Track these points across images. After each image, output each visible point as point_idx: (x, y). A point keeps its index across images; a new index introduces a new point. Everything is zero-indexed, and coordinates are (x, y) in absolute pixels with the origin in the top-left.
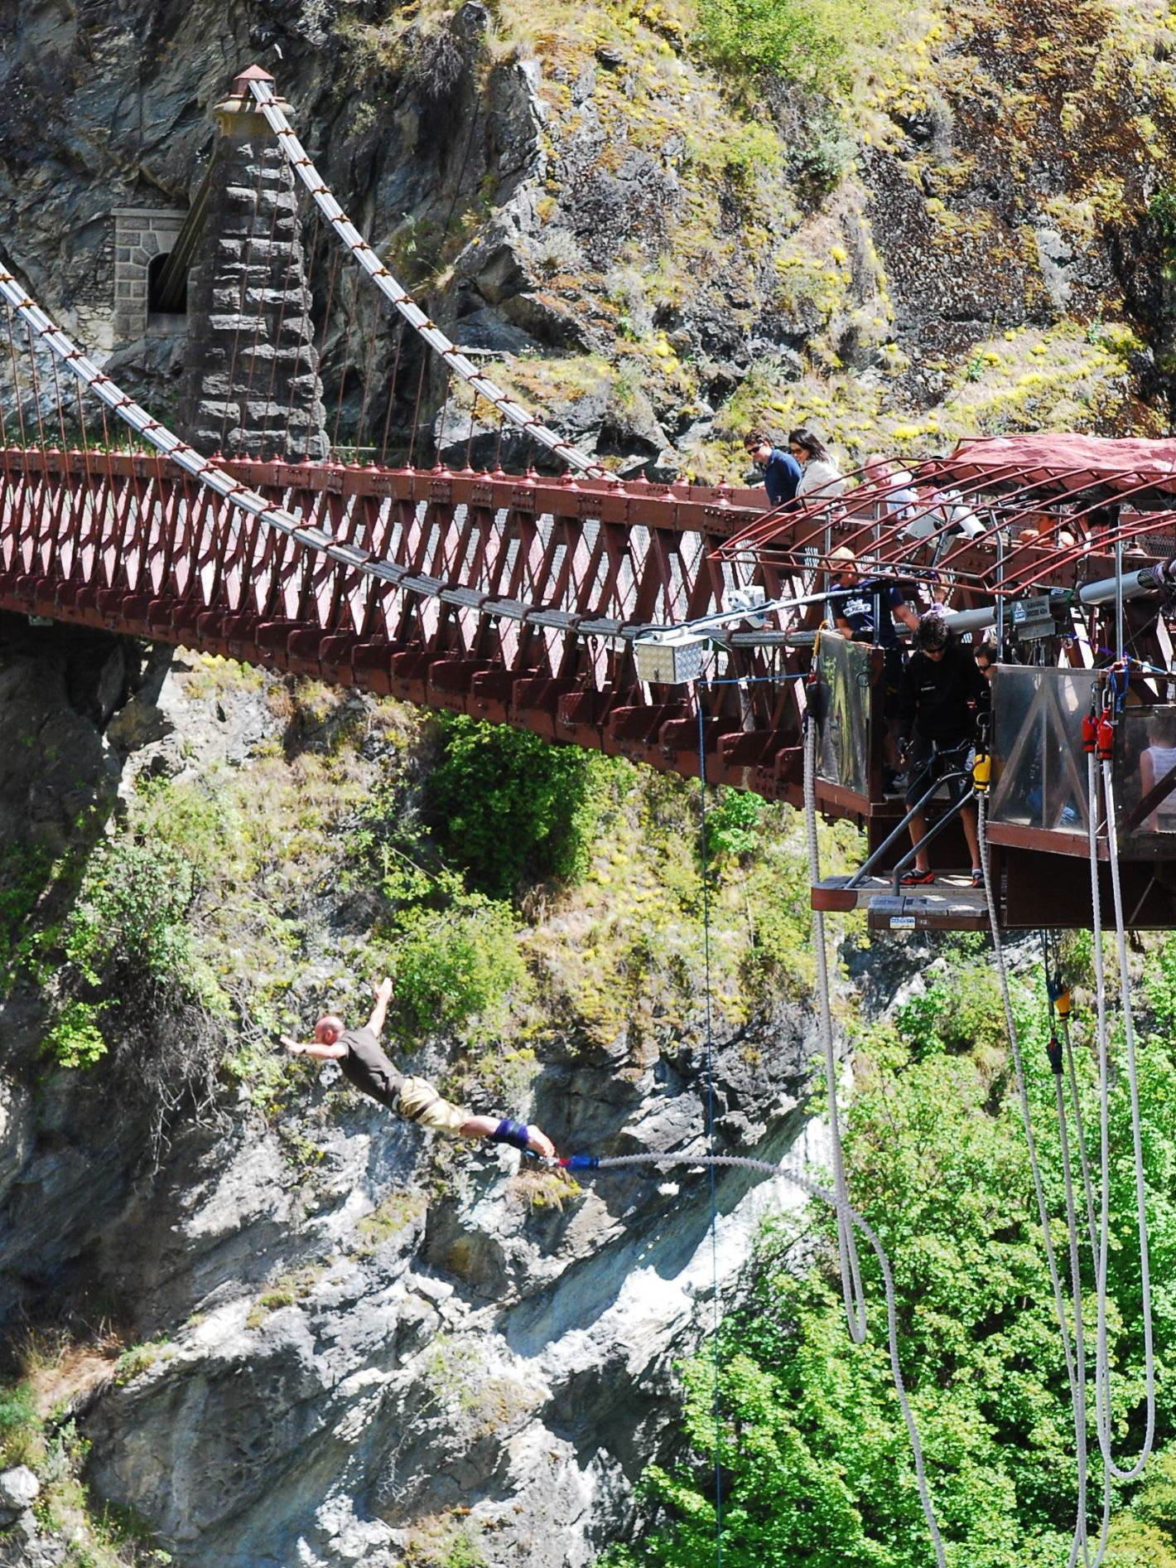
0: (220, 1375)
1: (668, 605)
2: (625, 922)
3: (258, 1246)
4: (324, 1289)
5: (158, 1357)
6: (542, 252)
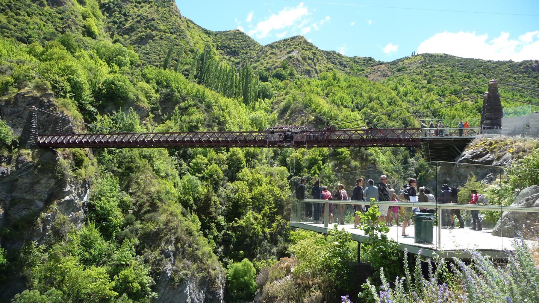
0: (68, 201)
1: (28, 92)
5: (63, 200)
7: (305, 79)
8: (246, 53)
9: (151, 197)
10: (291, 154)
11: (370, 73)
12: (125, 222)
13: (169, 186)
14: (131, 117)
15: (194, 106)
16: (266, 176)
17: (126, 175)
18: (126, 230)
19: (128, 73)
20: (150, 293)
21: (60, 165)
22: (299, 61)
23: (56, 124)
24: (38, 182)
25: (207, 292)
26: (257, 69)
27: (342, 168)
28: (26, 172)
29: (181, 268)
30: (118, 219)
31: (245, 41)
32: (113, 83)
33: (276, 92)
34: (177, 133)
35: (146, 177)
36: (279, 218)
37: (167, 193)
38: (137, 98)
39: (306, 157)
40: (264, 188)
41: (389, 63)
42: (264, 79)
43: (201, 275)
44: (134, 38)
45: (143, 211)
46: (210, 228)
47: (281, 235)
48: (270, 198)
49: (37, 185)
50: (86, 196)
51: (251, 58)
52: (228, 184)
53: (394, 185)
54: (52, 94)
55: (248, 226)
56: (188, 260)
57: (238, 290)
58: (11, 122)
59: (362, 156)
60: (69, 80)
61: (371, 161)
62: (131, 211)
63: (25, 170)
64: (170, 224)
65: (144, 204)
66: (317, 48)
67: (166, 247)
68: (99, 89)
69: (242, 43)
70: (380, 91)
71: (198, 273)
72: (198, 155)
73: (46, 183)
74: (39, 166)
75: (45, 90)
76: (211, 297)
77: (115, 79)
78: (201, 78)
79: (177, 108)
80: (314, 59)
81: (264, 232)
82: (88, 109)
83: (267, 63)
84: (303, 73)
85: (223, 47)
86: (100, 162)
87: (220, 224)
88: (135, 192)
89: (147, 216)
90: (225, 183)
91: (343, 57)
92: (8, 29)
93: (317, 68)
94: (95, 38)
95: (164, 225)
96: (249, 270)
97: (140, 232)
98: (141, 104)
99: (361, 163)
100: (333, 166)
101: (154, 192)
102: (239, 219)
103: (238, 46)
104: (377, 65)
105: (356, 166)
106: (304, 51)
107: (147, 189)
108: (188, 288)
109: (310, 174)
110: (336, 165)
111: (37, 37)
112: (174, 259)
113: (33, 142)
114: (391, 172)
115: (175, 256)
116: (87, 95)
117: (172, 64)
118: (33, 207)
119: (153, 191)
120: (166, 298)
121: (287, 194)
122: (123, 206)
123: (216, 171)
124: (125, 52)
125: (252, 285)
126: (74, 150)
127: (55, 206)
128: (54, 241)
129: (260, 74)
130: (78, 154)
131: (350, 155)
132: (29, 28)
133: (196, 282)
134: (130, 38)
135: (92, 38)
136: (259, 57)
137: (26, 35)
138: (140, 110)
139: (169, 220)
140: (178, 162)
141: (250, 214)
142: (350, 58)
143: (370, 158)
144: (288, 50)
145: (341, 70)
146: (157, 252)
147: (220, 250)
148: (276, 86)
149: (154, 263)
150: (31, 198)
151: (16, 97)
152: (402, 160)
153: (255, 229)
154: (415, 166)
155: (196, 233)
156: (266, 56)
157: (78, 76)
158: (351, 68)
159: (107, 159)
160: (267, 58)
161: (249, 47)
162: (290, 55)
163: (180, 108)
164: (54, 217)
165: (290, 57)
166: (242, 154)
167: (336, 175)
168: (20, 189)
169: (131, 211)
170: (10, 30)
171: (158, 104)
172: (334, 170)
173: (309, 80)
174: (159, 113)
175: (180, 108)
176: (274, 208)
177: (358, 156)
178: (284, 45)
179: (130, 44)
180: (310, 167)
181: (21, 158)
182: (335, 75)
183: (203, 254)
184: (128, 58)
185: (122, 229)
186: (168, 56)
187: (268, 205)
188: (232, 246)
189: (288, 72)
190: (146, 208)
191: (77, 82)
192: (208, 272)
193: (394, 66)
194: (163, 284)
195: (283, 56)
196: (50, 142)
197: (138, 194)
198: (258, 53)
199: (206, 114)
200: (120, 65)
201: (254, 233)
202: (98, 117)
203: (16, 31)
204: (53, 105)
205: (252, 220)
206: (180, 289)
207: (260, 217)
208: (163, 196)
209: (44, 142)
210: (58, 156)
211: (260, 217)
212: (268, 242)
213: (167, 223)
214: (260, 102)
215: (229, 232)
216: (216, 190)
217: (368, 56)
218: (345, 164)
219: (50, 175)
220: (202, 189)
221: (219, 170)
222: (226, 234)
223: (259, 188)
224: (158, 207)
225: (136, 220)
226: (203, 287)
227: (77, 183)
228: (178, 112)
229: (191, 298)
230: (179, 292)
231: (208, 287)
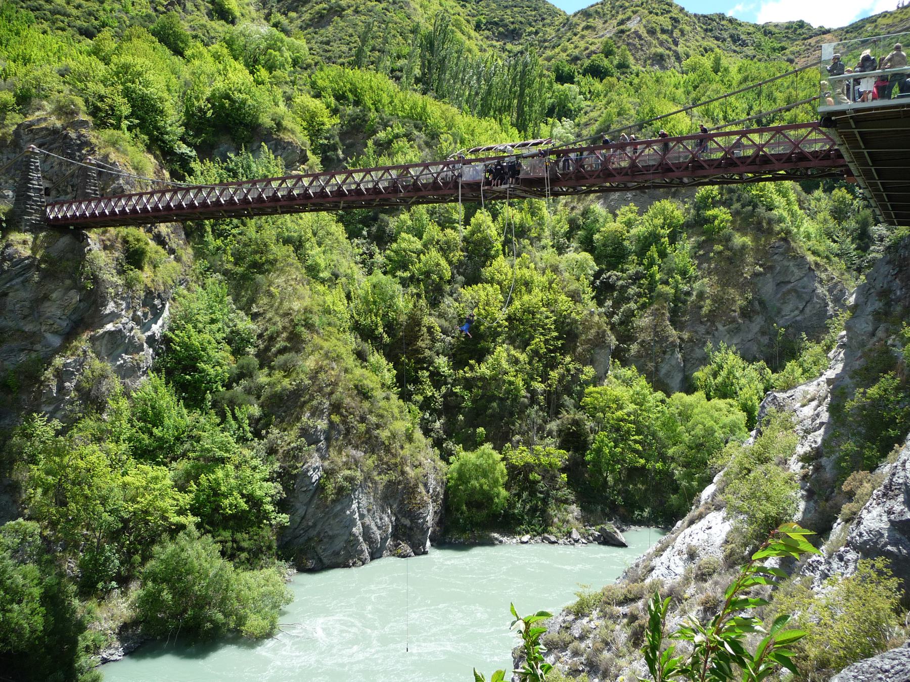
0: (110, 333)
1: (39, 121)
2: (145, 275)
3: (114, 317)
4: (123, 321)
5: (101, 331)
6: (276, 169)
7: (649, 74)
8: (536, 33)
9: (292, 320)
10: (604, 226)
11: (799, 53)
12: (236, 371)
13: (334, 298)
14: (265, 164)
15: (405, 135)
16: (544, 273)
17: (246, 278)
18: (238, 389)
19: (286, 83)
20: (273, 515)
21: (92, 262)
22: (640, 38)
23: (83, 177)
24: (46, 298)
25: (399, 512)
26: (553, 61)
27: (712, 251)
28: (21, 279)
29: (341, 464)
30: (218, 368)
31: (535, 9)
32: (227, 97)
33: (589, 103)
34: (278, 179)
35: (286, 281)
36: (568, 359)
37: (327, 311)
38: (279, 125)
39: (634, 231)
40: (535, 298)
41: (842, 29)
42: (563, 78)
43: (385, 478)
44: (307, 16)
45: (274, 350)
46: (417, 381)
47: (570, 395)
48: (547, 317)
49: (47, 304)
50: (160, 322)
51: (545, 41)
52: (461, 290)
53: (830, 284)
54: (86, 122)
55: (496, 379)
56: (356, 447)
57: (469, 504)
58: (11, 181)
59: (760, 223)
60: (127, 93)
61: (779, 233)
62: (251, 350)
63: (19, 275)
64: (322, 376)
65: (278, 336)
66: (682, 9)
67: (310, 423)
68: (200, 109)
69: (529, 13)
70: (814, 85)
71: (379, 474)
72: (403, 235)
73: (61, 299)
74: (43, 266)
75: (73, 113)
76: (407, 522)
77: (230, 89)
78: (428, 84)
79: (370, 143)
80: (672, 32)
81: (533, 392)
82: (178, 151)
83: (576, 47)
84: (649, 62)
85: (491, 23)
86: (199, 254)
87: (438, 374)
88: (265, 312)
89: (281, 359)
90: (456, 289)
91: (740, 25)
92: (65, 14)
93: (680, 49)
94: (233, 22)
95: (310, 379)
96: (492, 468)
97: (266, 392)
98: (287, 137)
99: (756, 239)
100: (694, 248)
101: (298, 311)
102: (479, 361)
103: (520, 19)
104: (816, 35)
105: (744, 247)
106: (653, 18)
107: (286, 305)
108: (355, 506)
109: (642, 267)
110: (700, 246)
111: (117, 24)
112: (328, 447)
113: (36, 217)
114: (827, 257)
115: (328, 439)
116: (172, 120)
117: (372, 59)
118: (38, 347)
119: (296, 308)
120: (310, 524)
121: (589, 311)
122: (236, 343)
123: (438, 265)
124: (282, 41)
125: (498, 495)
126: (123, 231)
127: (82, 343)
128: (81, 415)
129: (557, 70)
130: (131, 239)
131: (732, 222)
132: (104, 10)
133: (375, 493)
134: (300, 17)
135: (228, 22)
136: (560, 38)
137: (96, 23)
138: (284, 148)
139: (321, 367)
140: (368, 249)
141: (502, 353)
142: (755, 26)
143: (777, 228)
144: (620, 17)
145: (735, 51)
146: (294, 432)
147: (438, 424)
148: (590, 92)
149: (287, 454)
150: (35, 329)
151: (16, 133)
152: (855, 230)
153: (511, 383)
154: (887, 242)
155: (379, 394)
156: (575, 35)
157: (147, 84)
158: (758, 46)
159: (211, 247)
160: (575, 38)
161: (543, 19)
162: (622, 27)
163: (377, 143)
164: (81, 365)
165: (622, 32)
166: (493, 229)
167: (699, 267)
168: (12, 311)
169: (251, 350)
170: (69, 16)
171: (337, 139)
172: (694, 256)
173: (659, 73)
174: (338, 156)
175: (377, 143)
176: (557, 338)
177: (749, 224)
178: (613, 8)
179: (301, 27)
180: (642, 252)
181: (9, 251)
182: (717, 61)
183: (394, 436)
184: (287, 54)
185: (228, 386)
186: (364, 41)
187: (542, 334)
188: (461, 417)
189: (615, 62)
190: (280, 344)
191: (144, 98)
192: (403, 473)
193: (853, 35)
194: (303, 498)
195: (610, 32)
196: (65, 217)
197: (268, 315)
198: (559, 30)
199: (427, 150)
200: (271, 68)
201: (508, 392)
202: (196, 166)
203: (78, 18)
204: (88, 143)
205: (505, 365)
206: (339, 508)
207: (523, 357)
208: (316, 319)
209: (56, 218)
210: (89, 245)
211: (523, 357)
212: (541, 409)
213: (314, 376)
214: (553, 125)
215: (457, 390)
216: (434, 303)
217: (795, 18)
218: (720, 242)
219: (68, 282)
220: (403, 303)
221: (443, 262)
222: (450, 393)
223: (526, 298)
224: (303, 341)
225: (261, 367)
226: (391, 502)
227: (133, 298)
228: (371, 151)
229: (363, 524)
230: (336, 516)
231: (401, 502)
